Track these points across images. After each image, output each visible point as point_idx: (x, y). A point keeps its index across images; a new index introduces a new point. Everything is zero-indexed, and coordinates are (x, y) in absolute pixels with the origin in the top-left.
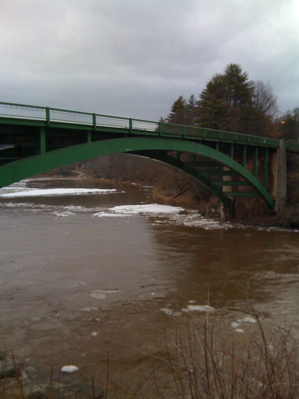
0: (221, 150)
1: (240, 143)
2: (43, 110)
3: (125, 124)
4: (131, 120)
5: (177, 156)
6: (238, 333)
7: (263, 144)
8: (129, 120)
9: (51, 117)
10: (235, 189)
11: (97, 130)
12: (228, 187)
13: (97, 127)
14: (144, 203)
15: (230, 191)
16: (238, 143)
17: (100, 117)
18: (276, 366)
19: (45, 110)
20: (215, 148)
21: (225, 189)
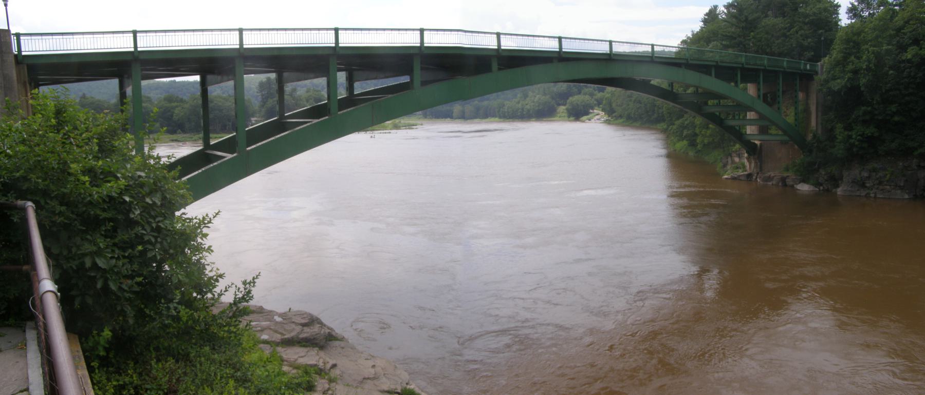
0: (718, 76)
1: (790, 70)
2: (555, 39)
3: (553, 46)
4: (498, 35)
5: (669, 85)
6: (833, 301)
7: (806, 70)
8: (608, 43)
9: (563, 47)
10: (763, 130)
11: (564, 56)
12: (754, 128)
13: (656, 57)
14: (168, 74)
15: (756, 132)
16: (767, 68)
17: (617, 43)
18: (30, 129)
19: (558, 39)
20: (710, 75)
21: (750, 130)
